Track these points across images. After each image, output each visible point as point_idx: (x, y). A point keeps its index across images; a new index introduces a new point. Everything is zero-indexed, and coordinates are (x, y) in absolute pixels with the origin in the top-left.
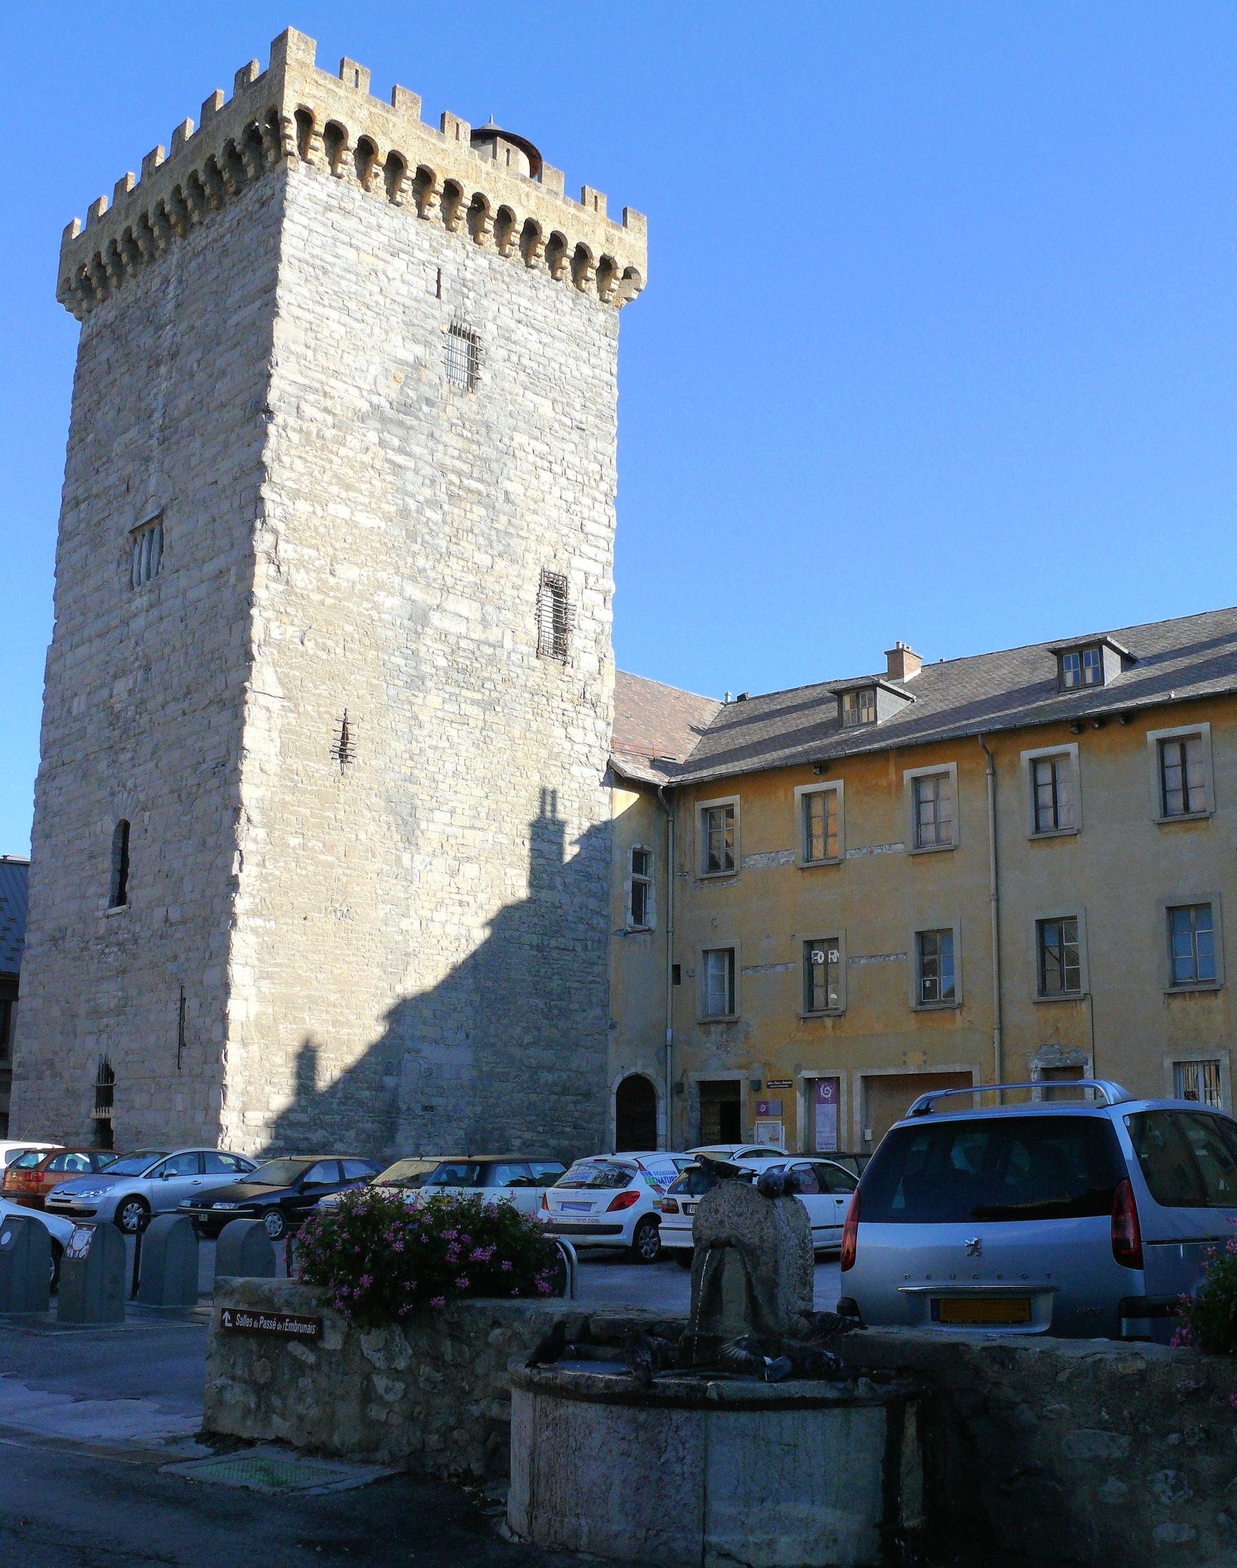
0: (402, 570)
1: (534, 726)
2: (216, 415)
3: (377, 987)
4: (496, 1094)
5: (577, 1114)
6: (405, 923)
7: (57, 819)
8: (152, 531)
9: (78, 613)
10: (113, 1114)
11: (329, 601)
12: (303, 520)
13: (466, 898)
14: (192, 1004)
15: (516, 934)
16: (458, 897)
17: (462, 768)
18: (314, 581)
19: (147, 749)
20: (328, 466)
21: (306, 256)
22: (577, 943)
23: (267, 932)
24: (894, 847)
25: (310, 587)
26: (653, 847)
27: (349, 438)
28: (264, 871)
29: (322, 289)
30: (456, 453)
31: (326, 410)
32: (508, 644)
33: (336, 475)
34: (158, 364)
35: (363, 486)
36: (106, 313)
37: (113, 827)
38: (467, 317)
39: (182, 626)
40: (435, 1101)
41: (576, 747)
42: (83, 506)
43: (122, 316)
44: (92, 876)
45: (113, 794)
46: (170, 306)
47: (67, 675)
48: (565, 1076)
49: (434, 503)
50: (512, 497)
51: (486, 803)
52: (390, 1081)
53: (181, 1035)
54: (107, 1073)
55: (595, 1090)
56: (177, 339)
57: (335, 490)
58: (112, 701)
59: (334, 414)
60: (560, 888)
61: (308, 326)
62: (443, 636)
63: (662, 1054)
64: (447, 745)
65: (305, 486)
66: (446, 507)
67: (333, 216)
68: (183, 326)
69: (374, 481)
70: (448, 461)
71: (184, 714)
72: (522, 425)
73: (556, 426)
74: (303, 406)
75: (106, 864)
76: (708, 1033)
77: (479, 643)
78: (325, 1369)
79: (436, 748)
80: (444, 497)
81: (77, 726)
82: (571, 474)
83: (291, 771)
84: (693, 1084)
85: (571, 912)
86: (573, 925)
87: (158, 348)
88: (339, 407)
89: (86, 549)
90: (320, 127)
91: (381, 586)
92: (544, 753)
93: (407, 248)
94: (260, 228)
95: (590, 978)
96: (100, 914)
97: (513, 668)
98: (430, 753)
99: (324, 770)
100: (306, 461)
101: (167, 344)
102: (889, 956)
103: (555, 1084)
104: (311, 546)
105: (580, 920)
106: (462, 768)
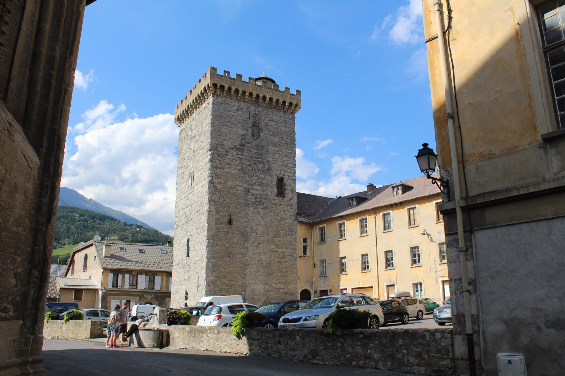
6: (246, 258)
10: (187, 301)
32: (269, 194)
36: (183, 126)
40: (255, 297)
54: (187, 293)
57: (226, 165)
62: (253, 195)
82: (284, 154)
90: (218, 87)
91: (237, 185)
92: (279, 218)
98: (251, 221)
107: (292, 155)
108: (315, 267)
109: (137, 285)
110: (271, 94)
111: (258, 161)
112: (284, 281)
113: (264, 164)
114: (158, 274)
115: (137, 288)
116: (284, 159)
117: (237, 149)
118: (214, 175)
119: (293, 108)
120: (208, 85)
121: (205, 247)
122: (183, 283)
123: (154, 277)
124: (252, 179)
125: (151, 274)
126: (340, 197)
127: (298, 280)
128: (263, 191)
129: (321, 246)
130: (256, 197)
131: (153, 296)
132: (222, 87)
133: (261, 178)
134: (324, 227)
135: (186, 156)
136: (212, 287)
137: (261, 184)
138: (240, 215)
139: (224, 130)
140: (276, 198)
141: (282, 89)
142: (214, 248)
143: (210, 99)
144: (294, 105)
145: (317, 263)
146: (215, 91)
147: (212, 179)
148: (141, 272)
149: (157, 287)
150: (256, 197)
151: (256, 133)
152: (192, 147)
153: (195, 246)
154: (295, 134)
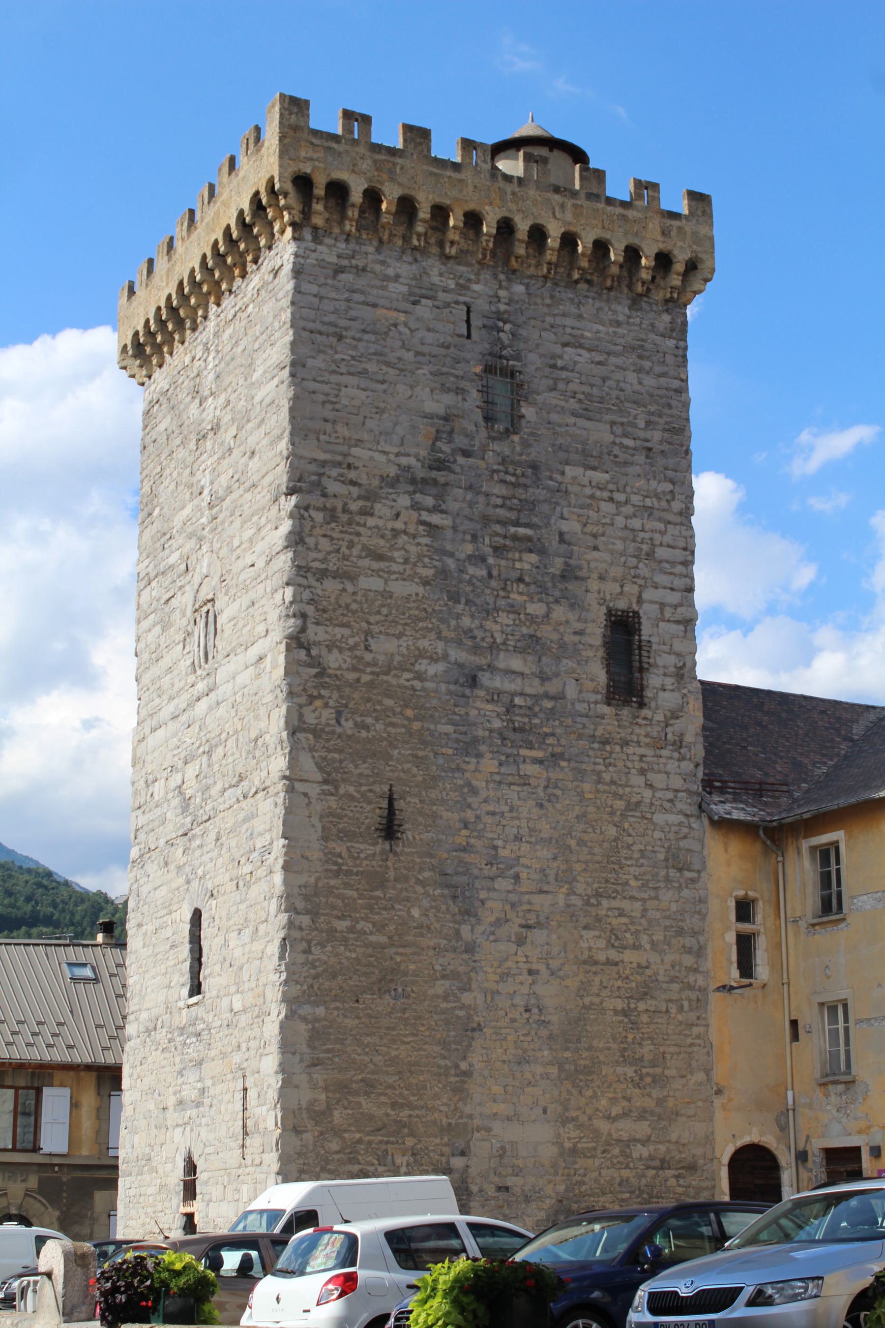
0: (444, 634)
1: (607, 777)
2: (248, 496)
3: (439, 1066)
4: (581, 1171)
5: (680, 1190)
6: (467, 998)
7: (146, 907)
8: (208, 612)
9: (155, 695)
10: (196, 1207)
11: (365, 678)
12: (333, 600)
13: (535, 967)
14: (252, 1094)
15: (597, 1000)
16: (528, 966)
17: (524, 831)
18: (349, 660)
19: (212, 836)
20: (356, 539)
21: (318, 326)
22: (670, 1005)
23: (317, 1020)
25: (344, 666)
27: (377, 506)
28: (311, 957)
29: (338, 357)
30: (499, 501)
31: (353, 483)
32: (571, 692)
33: (365, 548)
35: (396, 554)
36: (161, 378)
38: (504, 353)
40: (510, 1181)
41: (659, 794)
42: (154, 584)
45: (188, 882)
46: (211, 377)
47: (149, 759)
48: (663, 1148)
49: (479, 559)
50: (567, 537)
53: (244, 1126)
54: (191, 1168)
55: (701, 1162)
56: (218, 413)
57: (366, 562)
58: (184, 786)
59: (360, 485)
60: (648, 947)
61: (324, 398)
62: (494, 696)
64: (506, 809)
65: (333, 564)
66: (491, 560)
67: (347, 278)
68: (222, 400)
69: (407, 547)
70: (490, 511)
71: (238, 801)
72: (574, 457)
73: (616, 450)
74: (325, 481)
76: (827, 1095)
77: (536, 697)
79: (493, 814)
80: (488, 550)
81: (158, 812)
82: (636, 499)
83: (334, 855)
84: (817, 1152)
85: (662, 972)
86: (665, 986)
88: (364, 477)
90: (319, 191)
91: (421, 654)
92: (620, 804)
93: (430, 293)
95: (689, 1041)
96: (181, 1004)
97: (579, 719)
98: (489, 820)
99: (370, 850)
100: (332, 539)
101: (210, 418)
103: (651, 1158)
104: (343, 625)
105: (673, 980)
107: (677, 506)
108: (795, 1037)
110: (569, 216)
111: (515, 538)
113: (542, 552)
114: (58, 1076)
116: (636, 523)
117: (413, 481)
118: (310, 610)
119: (675, 280)
120: (271, 182)
121: (274, 948)
122: (172, 1117)
124: (489, 624)
128: (544, 678)
129: (824, 938)
130: (510, 708)
131: (33, 1182)
132: (338, 191)
134: (836, 845)
135: (177, 522)
136: (308, 1137)
137: (532, 645)
138: (434, 794)
139: (353, 394)
141: (619, 188)
142: (317, 950)
143: (284, 251)
144: (679, 267)
145: (809, 1017)
146: (306, 213)
147: (303, 630)
149: (54, 1139)
150: (510, 708)
151: (502, 404)
152: (205, 481)
154: (686, 405)
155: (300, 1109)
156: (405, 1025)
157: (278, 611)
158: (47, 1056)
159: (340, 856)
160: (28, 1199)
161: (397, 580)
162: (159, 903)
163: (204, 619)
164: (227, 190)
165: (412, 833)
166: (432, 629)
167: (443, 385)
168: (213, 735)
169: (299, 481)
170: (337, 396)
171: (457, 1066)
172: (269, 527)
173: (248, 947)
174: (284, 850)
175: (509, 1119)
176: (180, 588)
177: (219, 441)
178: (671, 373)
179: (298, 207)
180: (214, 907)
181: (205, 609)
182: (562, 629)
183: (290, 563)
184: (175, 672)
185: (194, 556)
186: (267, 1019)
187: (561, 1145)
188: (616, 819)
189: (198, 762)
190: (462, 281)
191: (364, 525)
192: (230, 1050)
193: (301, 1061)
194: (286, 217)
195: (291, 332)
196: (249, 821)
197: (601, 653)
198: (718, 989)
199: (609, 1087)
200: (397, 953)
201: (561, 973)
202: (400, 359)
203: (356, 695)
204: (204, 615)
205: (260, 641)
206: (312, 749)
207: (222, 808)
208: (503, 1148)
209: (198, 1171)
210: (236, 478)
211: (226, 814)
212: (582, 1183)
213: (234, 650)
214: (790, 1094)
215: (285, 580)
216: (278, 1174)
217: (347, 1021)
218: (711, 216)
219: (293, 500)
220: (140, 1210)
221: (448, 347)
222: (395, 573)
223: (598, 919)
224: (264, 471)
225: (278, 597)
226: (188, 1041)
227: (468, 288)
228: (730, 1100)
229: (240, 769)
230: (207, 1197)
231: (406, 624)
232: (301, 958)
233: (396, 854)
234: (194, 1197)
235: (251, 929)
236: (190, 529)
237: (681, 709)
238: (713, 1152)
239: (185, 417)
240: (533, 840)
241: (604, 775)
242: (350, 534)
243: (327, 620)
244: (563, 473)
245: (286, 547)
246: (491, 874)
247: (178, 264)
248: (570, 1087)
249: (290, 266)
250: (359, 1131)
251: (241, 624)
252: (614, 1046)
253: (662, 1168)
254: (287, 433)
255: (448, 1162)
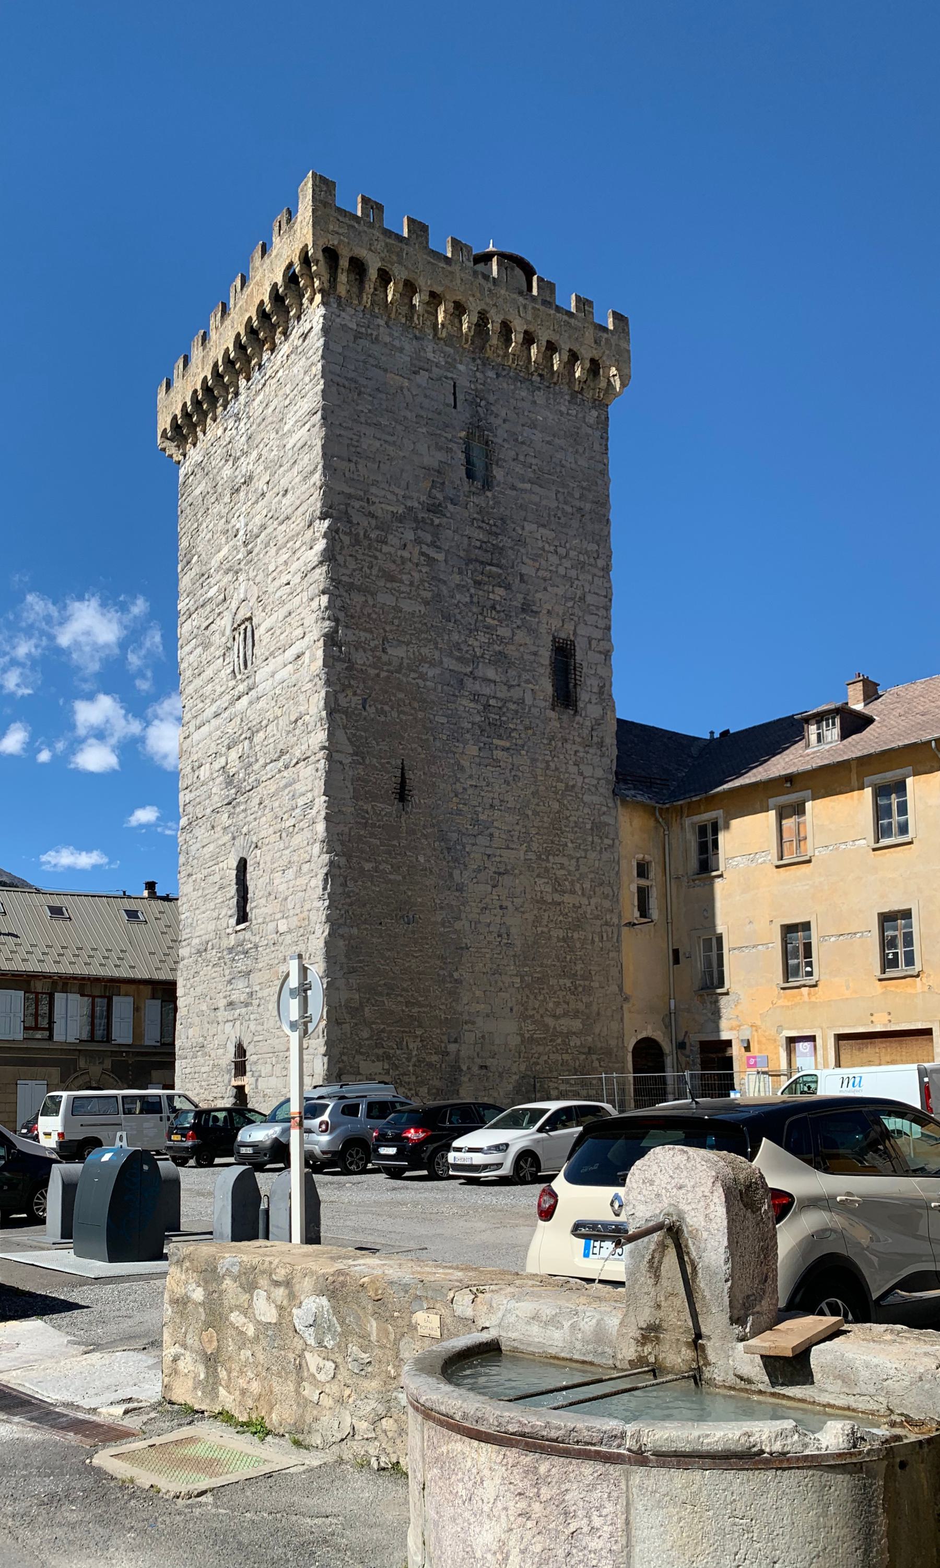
1: (552, 765)
2: (283, 527)
4: (536, 1055)
6: (458, 925)
7: (196, 861)
8: (245, 629)
9: (198, 701)
10: (247, 1081)
11: (384, 674)
13: (504, 904)
15: (546, 930)
17: (496, 802)
18: (370, 658)
24: (857, 843)
25: (368, 663)
26: (652, 857)
27: (390, 537)
28: (347, 890)
30: (478, 544)
32: (529, 700)
34: (238, 490)
35: (404, 577)
37: (235, 864)
39: (273, 703)
42: (194, 616)
43: (207, 454)
44: (223, 902)
45: (234, 838)
47: (194, 750)
50: (525, 578)
51: (517, 828)
52: (452, 1048)
54: (241, 1051)
57: (381, 583)
58: (228, 767)
59: (377, 518)
61: (349, 442)
62: (475, 697)
63: (667, 1020)
68: (254, 454)
69: (413, 573)
75: (233, 889)
77: (505, 701)
78: (264, 1342)
85: (589, 911)
87: (236, 477)
89: (200, 649)
90: (344, 263)
91: (423, 660)
92: (561, 786)
94: (304, 359)
98: (470, 791)
99: (389, 809)
101: (244, 472)
102: (855, 934)
104: (365, 630)
106: (496, 802)
107: (601, 563)
109: (50, 1029)
112: (581, 1007)
113: (508, 587)
114: (124, 988)
115: (51, 1037)
117: (416, 520)
118: (341, 615)
121: (318, 882)
122: (222, 1014)
123: (110, 1000)
124: (471, 641)
125: (101, 990)
126: (725, 733)
127: (626, 1006)
129: (535, 1210)
130: (487, 706)
131: (108, 1064)
132: (358, 267)
133: (501, 639)
135: (214, 563)
136: (347, 1027)
137: (500, 659)
140: (552, 715)
143: (314, 315)
148: (65, 983)
149: (122, 1033)
151: (479, 464)
152: (240, 524)
153: (271, 882)
154: (607, 485)
155: (340, 1006)
156: (415, 944)
157: (315, 615)
158: (116, 973)
159: (367, 813)
160: (104, 1076)
161: (405, 598)
162: (207, 856)
163: (242, 636)
164: (261, 270)
165: (417, 798)
166: (430, 641)
167: (437, 444)
168: (254, 723)
169: (331, 508)
170: (358, 441)
171: (451, 976)
172: (304, 548)
173: (291, 884)
174: (326, 805)
175: (488, 1016)
176: (219, 614)
177: (253, 489)
178: (598, 458)
179: (326, 277)
180: (258, 855)
181: (243, 627)
182: (522, 649)
183: (324, 575)
184: (217, 681)
185: (232, 587)
186: (312, 937)
187: (522, 1035)
188: (558, 797)
189: (241, 746)
190: (449, 360)
191: (381, 551)
192: (276, 962)
193: (342, 968)
194: (317, 283)
195: (322, 382)
196: (290, 785)
197: (548, 670)
198: (626, 925)
199: (554, 993)
200: (408, 889)
201: (522, 909)
202: (405, 417)
203: (377, 687)
204: (242, 632)
205: (298, 643)
206: (345, 728)
207: (264, 778)
208: (483, 1037)
209: (247, 1054)
210: (270, 515)
211: (268, 783)
212: (537, 1064)
213: (272, 654)
214: (672, 1001)
215: (321, 588)
216: (324, 1055)
217: (374, 940)
218: (628, 334)
219: (327, 523)
220: (195, 1084)
221: (439, 414)
222: (403, 593)
223: (547, 870)
224: (298, 502)
225: (314, 604)
226: (237, 958)
227: (455, 367)
228: (633, 1005)
229: (280, 746)
230: (256, 1074)
231: (411, 634)
232: (340, 890)
233: (407, 813)
234: (243, 1073)
235: (295, 868)
236: (226, 566)
237: (603, 718)
238: (623, 1043)
239: (219, 478)
240: (503, 808)
241: (551, 763)
242: (370, 556)
243: (354, 624)
244: (523, 529)
245: (321, 563)
246: (475, 833)
247: (213, 349)
248: (528, 993)
249: (320, 326)
250: (383, 1023)
251: (278, 632)
252: (558, 964)
253: (589, 1053)
254: (320, 466)
255: (446, 1047)
